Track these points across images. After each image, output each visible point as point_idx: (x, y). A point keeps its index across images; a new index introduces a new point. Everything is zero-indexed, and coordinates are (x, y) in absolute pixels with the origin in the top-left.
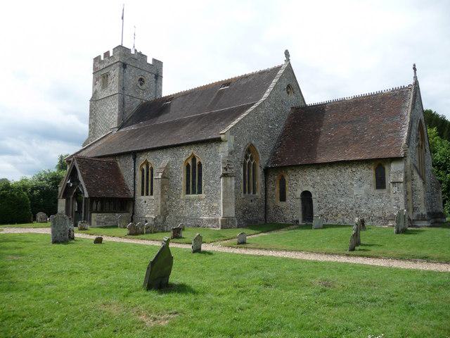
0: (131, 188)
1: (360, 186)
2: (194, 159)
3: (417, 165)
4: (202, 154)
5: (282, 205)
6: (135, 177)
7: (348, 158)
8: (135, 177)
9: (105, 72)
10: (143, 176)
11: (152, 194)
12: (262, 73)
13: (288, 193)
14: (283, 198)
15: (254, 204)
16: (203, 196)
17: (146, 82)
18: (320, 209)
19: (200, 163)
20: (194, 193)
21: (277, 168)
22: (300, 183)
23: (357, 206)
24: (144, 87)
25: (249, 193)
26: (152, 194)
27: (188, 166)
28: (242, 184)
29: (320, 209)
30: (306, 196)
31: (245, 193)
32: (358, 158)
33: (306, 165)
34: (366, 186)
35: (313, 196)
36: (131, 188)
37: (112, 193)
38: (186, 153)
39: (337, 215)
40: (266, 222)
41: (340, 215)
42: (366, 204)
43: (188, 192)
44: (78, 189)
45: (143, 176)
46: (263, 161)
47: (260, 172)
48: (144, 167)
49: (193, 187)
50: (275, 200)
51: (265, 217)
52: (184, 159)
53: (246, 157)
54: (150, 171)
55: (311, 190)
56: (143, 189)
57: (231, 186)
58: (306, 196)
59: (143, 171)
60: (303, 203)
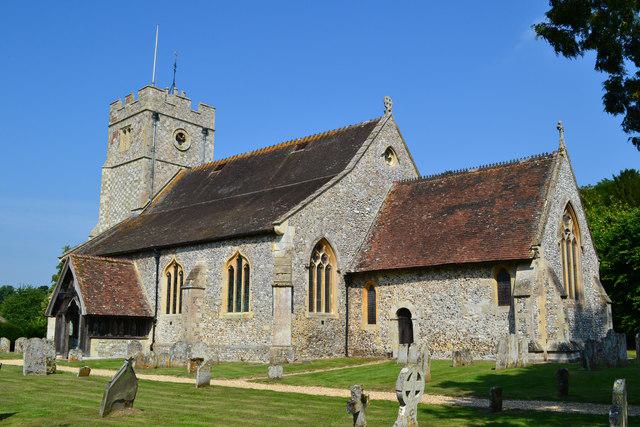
0: (151, 302)
1: (476, 302)
2: (240, 259)
3: (559, 271)
4: (250, 250)
5: (371, 328)
6: (157, 287)
7: (227, 297)
8: (157, 287)
9: (126, 123)
10: (169, 284)
11: (246, 310)
12: (340, 134)
13: (378, 311)
14: (372, 320)
15: (327, 328)
16: (250, 314)
17: (187, 139)
18: (422, 335)
19: (247, 265)
20: (238, 309)
21: (365, 273)
22: (395, 297)
23: (472, 330)
24: (185, 146)
25: (319, 309)
26: (246, 310)
27: (231, 270)
28: (307, 297)
29: (422, 335)
30: (404, 315)
31: (311, 310)
32: (475, 260)
33: (403, 270)
34: (485, 302)
35: (413, 316)
36: (151, 302)
37: (122, 309)
38: (228, 251)
39: (445, 345)
40: (347, 355)
41: (449, 345)
42: (484, 328)
43: (230, 309)
44: (74, 302)
45: (169, 284)
46: (342, 262)
47: (337, 280)
48: (172, 271)
49: (237, 302)
50: (359, 322)
51: (346, 348)
52: (226, 260)
53: (314, 256)
54: (179, 277)
55: (410, 307)
56: (168, 304)
57: (286, 301)
58: (404, 315)
59: (169, 276)
60: (400, 325)
